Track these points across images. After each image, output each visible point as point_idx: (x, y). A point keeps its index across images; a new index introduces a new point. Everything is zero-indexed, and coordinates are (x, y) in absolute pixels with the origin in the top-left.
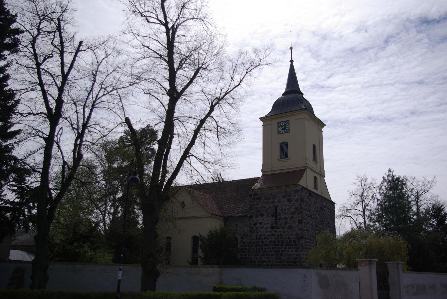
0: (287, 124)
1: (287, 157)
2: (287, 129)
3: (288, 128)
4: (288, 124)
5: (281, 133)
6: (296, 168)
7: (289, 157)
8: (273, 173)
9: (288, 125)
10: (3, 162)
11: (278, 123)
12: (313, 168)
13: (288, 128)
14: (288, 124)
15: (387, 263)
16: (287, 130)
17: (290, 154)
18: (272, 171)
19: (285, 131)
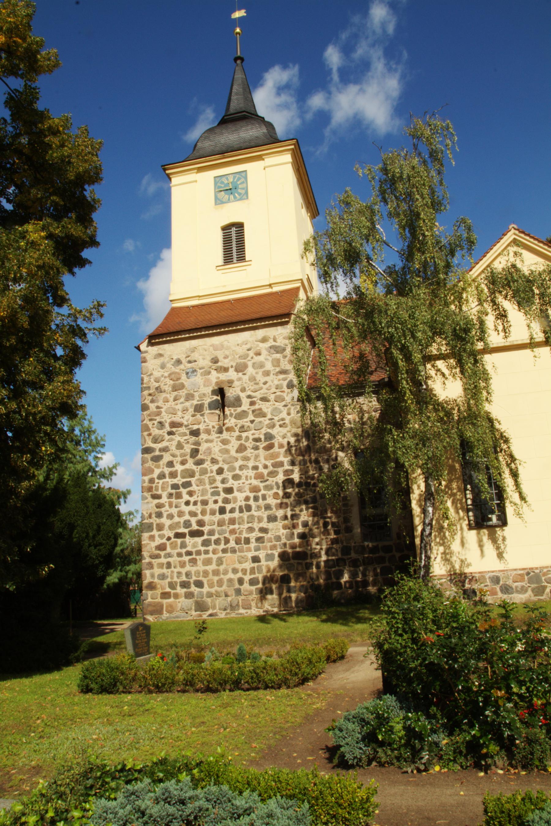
0: (239, 179)
1: (242, 258)
2: (240, 191)
3: (243, 189)
4: (243, 180)
5: (222, 203)
6: (199, 296)
7: (247, 259)
8: (276, 289)
9: (243, 183)
10: (462, 687)
11: (215, 177)
12: (225, 286)
13: (243, 189)
14: (243, 180)
15: (53, 521)
16: (240, 194)
17: (249, 253)
18: (270, 285)
19: (235, 197)
